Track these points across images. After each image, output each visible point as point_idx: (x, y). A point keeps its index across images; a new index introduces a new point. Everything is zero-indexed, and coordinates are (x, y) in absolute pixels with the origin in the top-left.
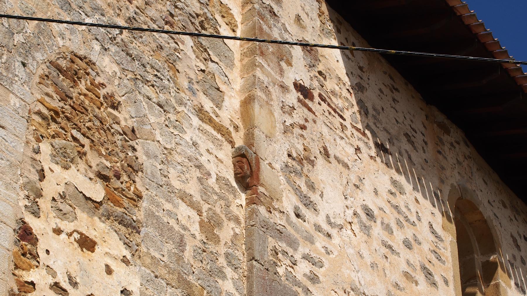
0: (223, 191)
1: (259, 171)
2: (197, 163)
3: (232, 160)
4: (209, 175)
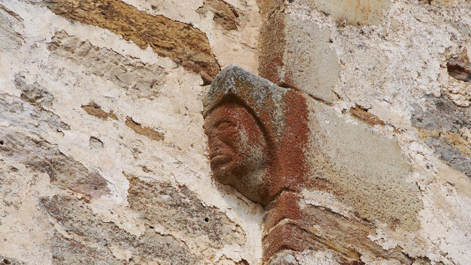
0: (159, 228)
1: (305, 139)
2: (41, 155)
3: (202, 122)
4: (98, 184)
